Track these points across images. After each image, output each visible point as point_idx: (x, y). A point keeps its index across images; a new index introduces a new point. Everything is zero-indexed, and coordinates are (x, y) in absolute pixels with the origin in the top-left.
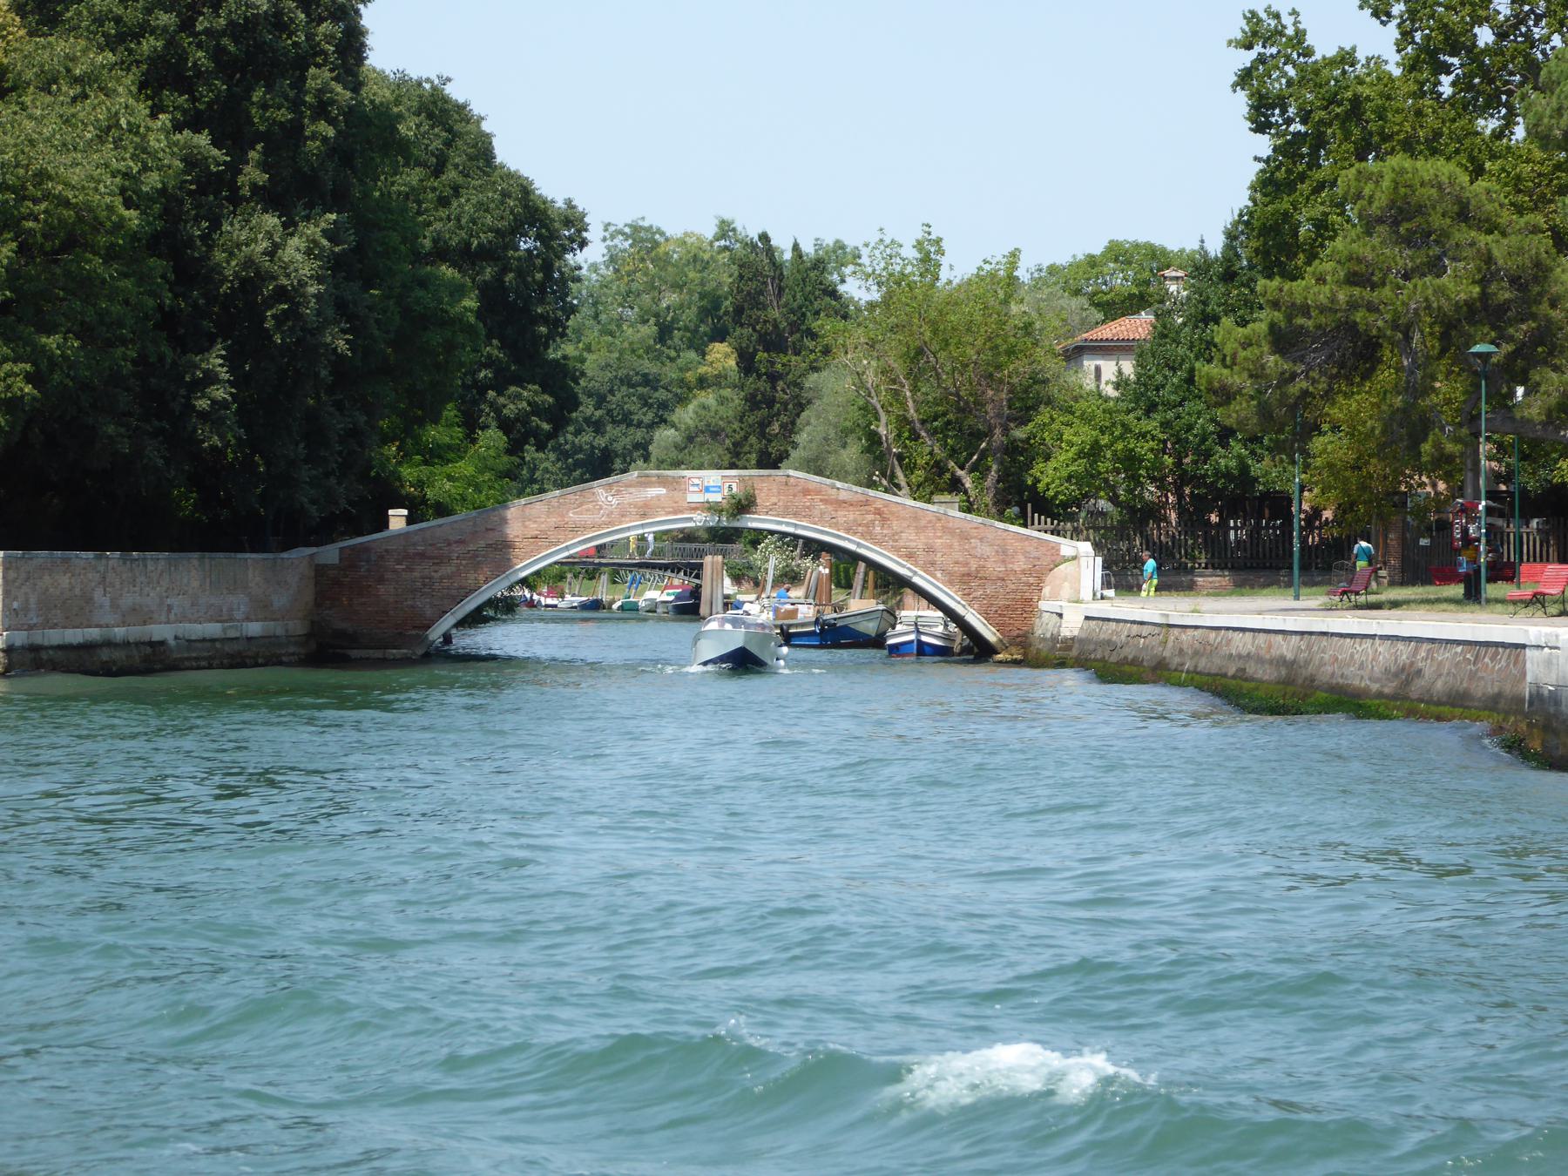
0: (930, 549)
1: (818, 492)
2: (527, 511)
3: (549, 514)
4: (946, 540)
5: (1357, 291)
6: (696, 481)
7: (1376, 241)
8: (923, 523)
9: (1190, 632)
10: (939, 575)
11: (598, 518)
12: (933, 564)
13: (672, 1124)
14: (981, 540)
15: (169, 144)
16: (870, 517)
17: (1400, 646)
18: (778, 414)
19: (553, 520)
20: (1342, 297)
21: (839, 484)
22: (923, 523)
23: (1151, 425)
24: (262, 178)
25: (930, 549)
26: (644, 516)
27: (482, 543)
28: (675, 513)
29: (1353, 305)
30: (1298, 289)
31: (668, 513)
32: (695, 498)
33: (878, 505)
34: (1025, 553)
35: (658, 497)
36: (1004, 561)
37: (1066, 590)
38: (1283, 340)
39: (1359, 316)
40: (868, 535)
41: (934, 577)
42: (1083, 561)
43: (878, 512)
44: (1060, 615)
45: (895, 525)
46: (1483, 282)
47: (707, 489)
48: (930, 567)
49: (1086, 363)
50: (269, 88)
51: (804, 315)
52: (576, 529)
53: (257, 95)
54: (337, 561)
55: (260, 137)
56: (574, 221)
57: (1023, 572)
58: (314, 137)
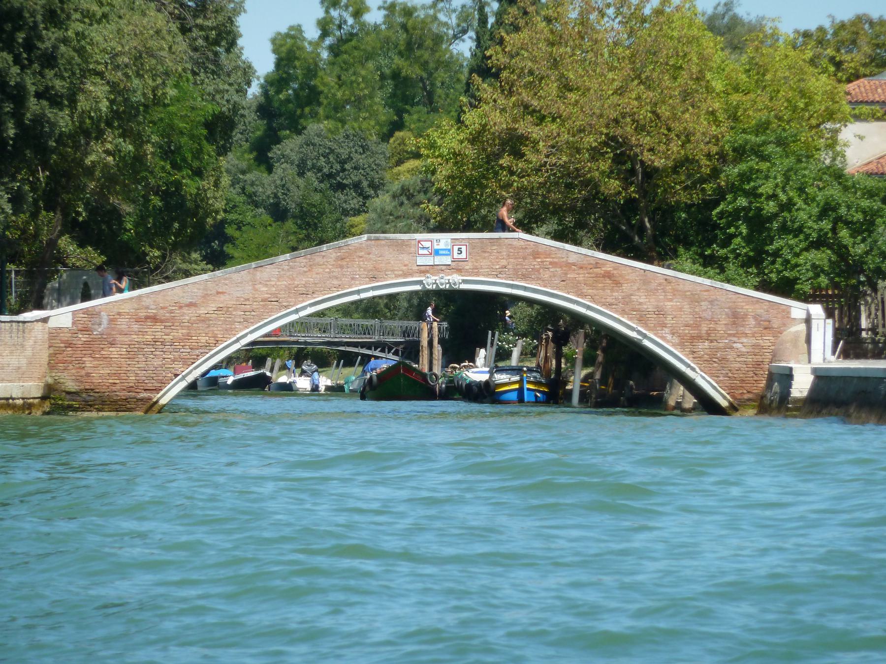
6: (428, 244)
8: (653, 285)
10: (669, 337)
13: (38, 444)
22: (653, 285)
25: (660, 312)
26: (374, 278)
27: (213, 306)
28: (405, 275)
31: (397, 276)
47: (437, 253)
54: (70, 325)
56: (298, 29)
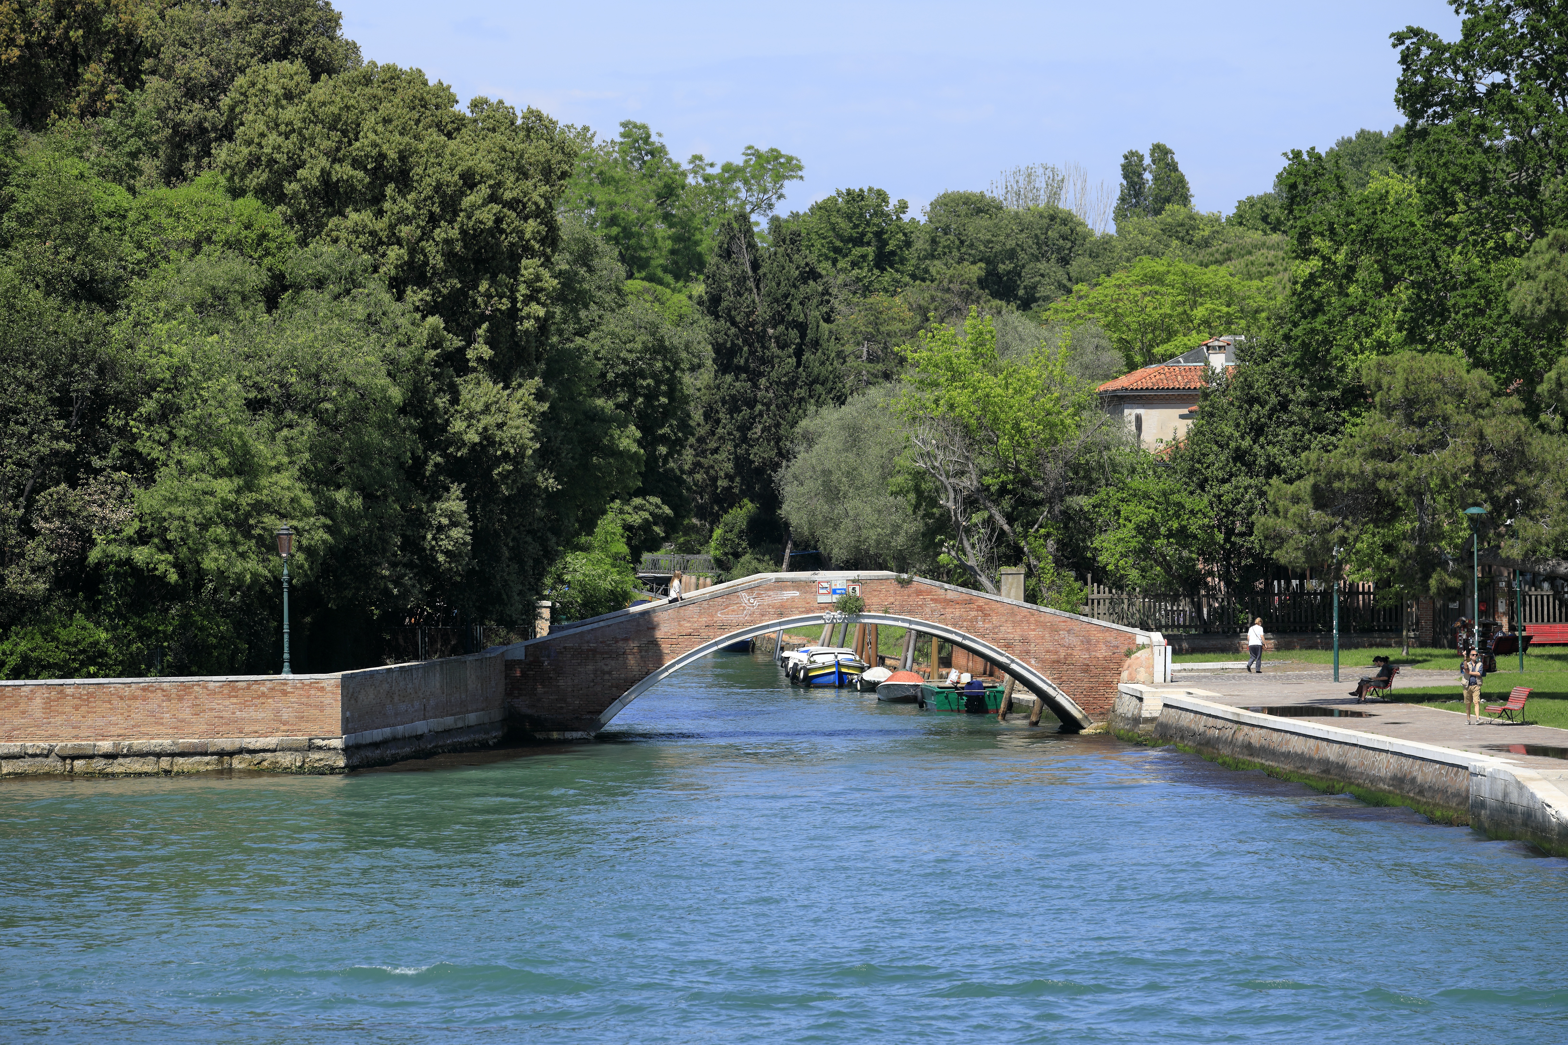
0: (1025, 641)
1: (929, 593)
2: (682, 611)
3: (700, 614)
4: (1039, 632)
5: (1380, 465)
7: (1394, 421)
8: (1018, 618)
9: (1257, 730)
11: (741, 618)
12: (1028, 652)
14: (1069, 631)
15: (416, 327)
16: (973, 614)
17: (1403, 759)
18: (761, 414)
19: (704, 620)
20: (1368, 467)
21: (946, 586)
22: (1018, 618)
23: (1201, 502)
24: (487, 352)
25: (1025, 641)
26: (781, 615)
29: (1377, 475)
30: (1335, 460)
32: (824, 599)
33: (981, 603)
34: (1106, 643)
35: (793, 598)
36: (1088, 650)
37: (1142, 675)
38: (1322, 498)
39: (1381, 485)
40: (972, 628)
41: (1029, 663)
42: (1156, 649)
43: (980, 609)
44: (1141, 699)
45: (995, 619)
46: (1478, 454)
48: (1025, 654)
49: (1127, 412)
50: (493, 281)
51: (789, 307)
52: (723, 628)
53: (484, 286)
55: (483, 318)
57: (1105, 658)
58: (528, 317)
